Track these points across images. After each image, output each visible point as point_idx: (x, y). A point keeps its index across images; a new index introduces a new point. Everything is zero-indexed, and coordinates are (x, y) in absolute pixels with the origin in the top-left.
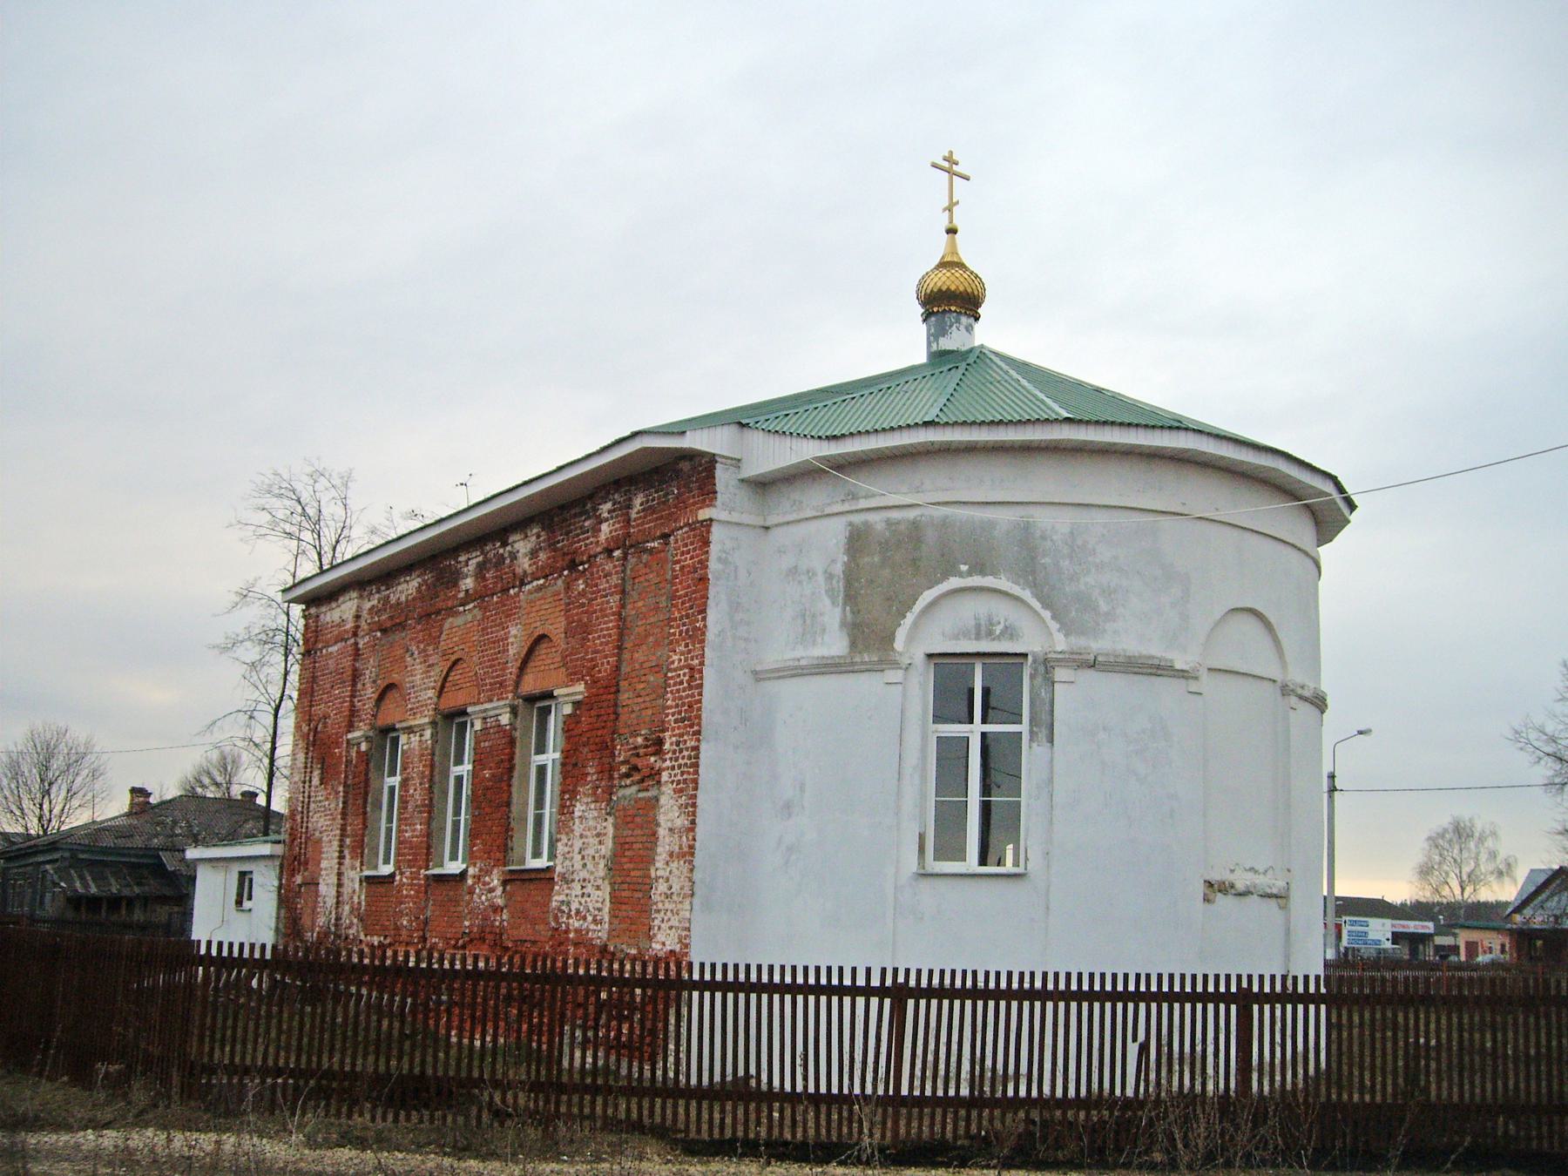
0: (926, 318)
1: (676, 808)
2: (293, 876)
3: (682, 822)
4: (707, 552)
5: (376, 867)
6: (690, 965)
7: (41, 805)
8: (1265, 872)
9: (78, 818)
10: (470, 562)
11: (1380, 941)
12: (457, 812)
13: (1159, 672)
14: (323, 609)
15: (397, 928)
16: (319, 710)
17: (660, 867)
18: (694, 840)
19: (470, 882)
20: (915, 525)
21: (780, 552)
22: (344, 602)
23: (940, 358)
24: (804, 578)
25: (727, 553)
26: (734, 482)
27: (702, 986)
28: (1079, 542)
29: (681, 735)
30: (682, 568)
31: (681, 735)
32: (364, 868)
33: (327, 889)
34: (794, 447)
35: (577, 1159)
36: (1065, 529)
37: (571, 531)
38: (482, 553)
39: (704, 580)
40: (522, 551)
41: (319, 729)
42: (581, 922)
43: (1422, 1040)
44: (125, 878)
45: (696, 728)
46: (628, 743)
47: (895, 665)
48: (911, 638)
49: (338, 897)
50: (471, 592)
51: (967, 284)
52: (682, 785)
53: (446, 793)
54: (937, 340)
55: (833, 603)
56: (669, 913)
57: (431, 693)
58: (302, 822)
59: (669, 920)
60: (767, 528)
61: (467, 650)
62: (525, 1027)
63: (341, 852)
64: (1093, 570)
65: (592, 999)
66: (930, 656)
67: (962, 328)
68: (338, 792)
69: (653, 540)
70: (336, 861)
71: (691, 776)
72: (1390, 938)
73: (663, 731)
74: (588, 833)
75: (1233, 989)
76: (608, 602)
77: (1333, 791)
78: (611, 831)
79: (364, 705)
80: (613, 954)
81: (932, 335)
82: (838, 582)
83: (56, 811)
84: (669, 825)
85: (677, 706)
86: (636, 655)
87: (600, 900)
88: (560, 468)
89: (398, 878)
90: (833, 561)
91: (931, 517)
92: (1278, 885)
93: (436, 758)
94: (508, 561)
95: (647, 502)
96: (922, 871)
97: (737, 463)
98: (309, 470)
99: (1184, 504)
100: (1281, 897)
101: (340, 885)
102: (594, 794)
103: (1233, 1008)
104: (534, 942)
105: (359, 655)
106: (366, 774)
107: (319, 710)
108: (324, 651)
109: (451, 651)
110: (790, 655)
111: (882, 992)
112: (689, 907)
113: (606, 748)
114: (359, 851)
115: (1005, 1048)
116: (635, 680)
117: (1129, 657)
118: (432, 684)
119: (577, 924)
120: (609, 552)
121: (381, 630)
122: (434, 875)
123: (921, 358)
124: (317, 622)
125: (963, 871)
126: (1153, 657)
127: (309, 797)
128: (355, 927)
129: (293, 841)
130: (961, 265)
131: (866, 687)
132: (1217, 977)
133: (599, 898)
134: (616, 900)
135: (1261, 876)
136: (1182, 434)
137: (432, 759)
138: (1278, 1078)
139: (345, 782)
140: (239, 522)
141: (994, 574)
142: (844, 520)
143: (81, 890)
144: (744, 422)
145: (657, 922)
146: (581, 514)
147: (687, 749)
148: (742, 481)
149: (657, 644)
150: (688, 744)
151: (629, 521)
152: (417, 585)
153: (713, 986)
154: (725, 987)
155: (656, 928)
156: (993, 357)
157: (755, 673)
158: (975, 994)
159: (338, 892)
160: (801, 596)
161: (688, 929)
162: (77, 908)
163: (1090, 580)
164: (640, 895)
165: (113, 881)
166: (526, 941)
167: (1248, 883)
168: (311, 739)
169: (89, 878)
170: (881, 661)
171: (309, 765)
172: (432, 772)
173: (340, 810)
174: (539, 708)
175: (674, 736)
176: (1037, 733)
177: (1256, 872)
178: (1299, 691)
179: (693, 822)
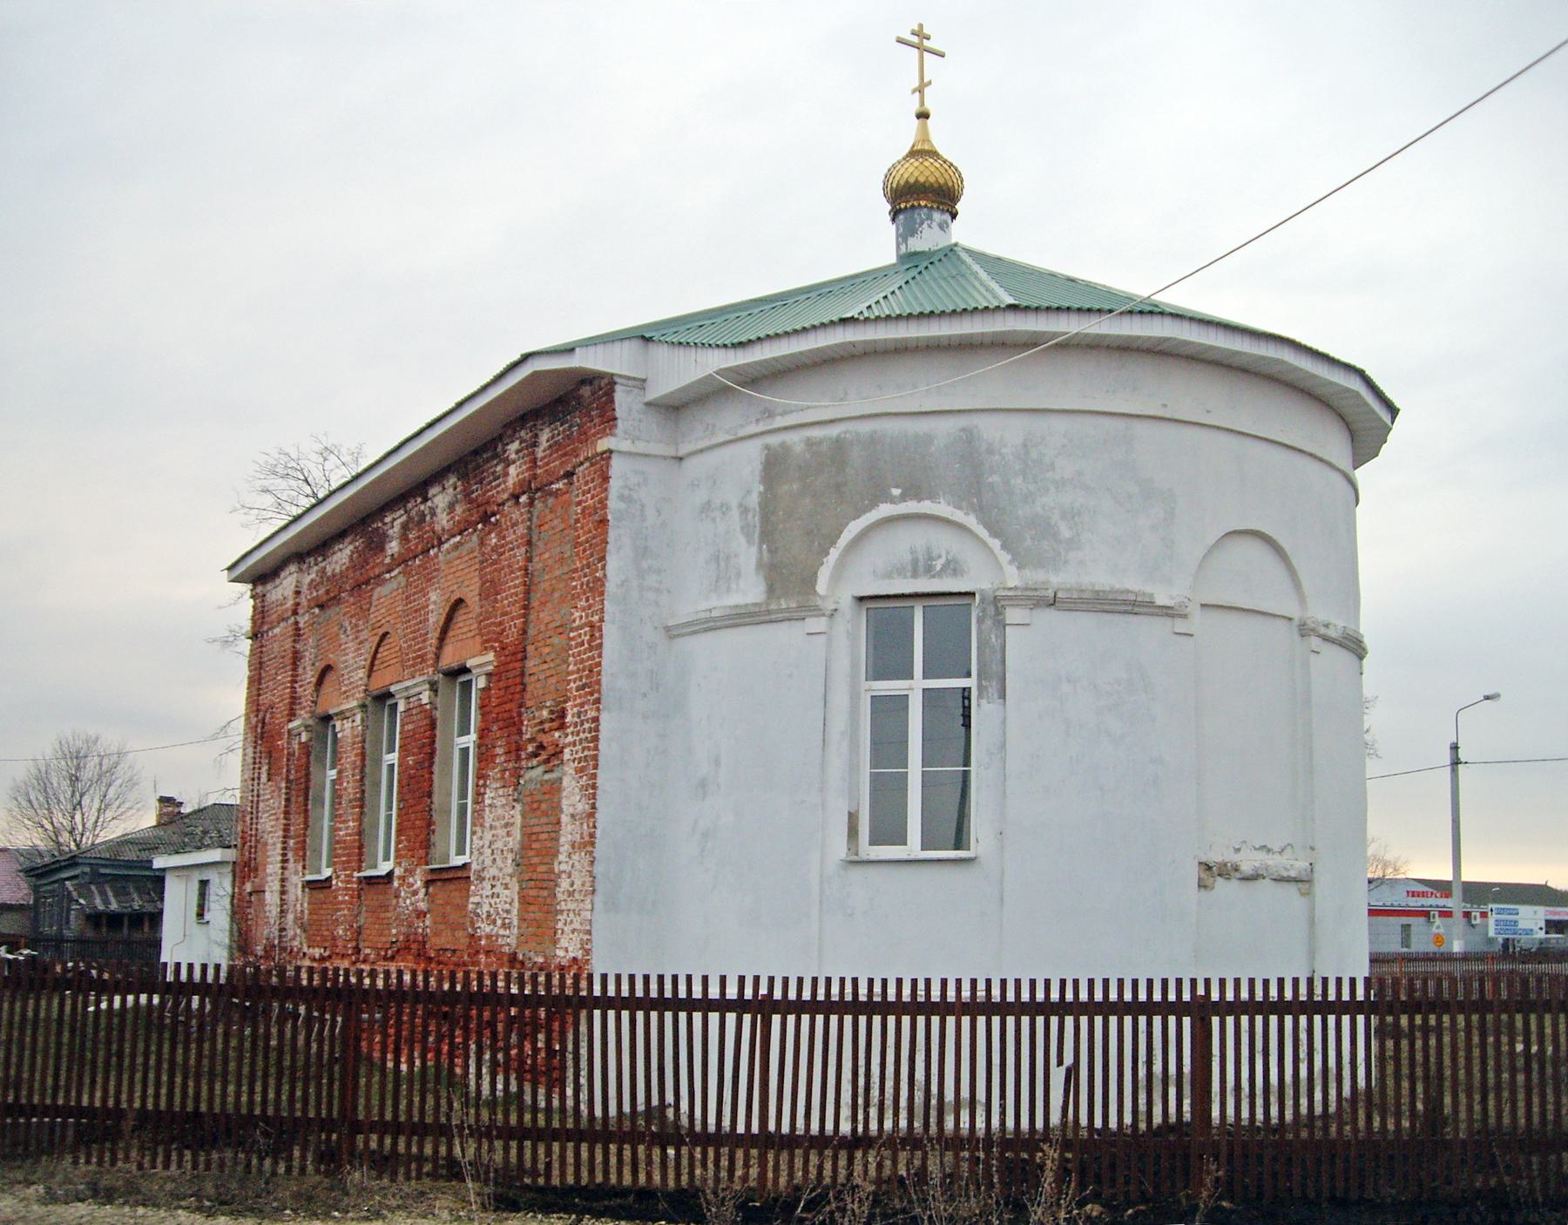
0: (895, 214)
1: (577, 790)
2: (244, 883)
3: (583, 807)
4: (606, 489)
5: (319, 872)
6: (590, 977)
7: (73, 818)
8: (1281, 852)
9: (113, 831)
10: (394, 522)
11: (1532, 930)
12: (390, 808)
13: (1136, 610)
14: (269, 586)
15: (334, 938)
16: (265, 699)
17: (563, 863)
18: (595, 827)
19: (396, 884)
20: (839, 445)
21: (693, 485)
22: (285, 578)
23: (910, 260)
24: (717, 514)
25: (630, 489)
26: (641, 406)
27: (605, 1003)
28: (1034, 455)
29: (582, 705)
30: (584, 510)
31: (582, 705)
32: (307, 872)
33: (271, 898)
34: (699, 360)
35: (350, 1215)
37: (484, 479)
38: (406, 512)
39: (603, 522)
40: (441, 505)
41: (267, 720)
42: (491, 927)
43: (1519, 1047)
44: (149, 894)
45: (596, 695)
46: (534, 718)
47: (817, 611)
48: (837, 577)
49: (282, 905)
50: (396, 556)
51: (938, 174)
52: (582, 764)
53: (378, 784)
54: (905, 241)
55: (748, 542)
56: (571, 915)
57: (361, 673)
58: (252, 824)
59: (571, 922)
60: (681, 459)
61: (392, 622)
62: (445, 1048)
63: (284, 855)
65: (501, 1016)
66: (861, 599)
67: (934, 225)
68: (280, 789)
69: (558, 480)
70: (279, 865)
71: (592, 753)
72: (1543, 926)
73: (565, 702)
74: (497, 824)
75: (1186, 997)
76: (515, 556)
77: (1457, 763)
78: (518, 820)
79: (305, 690)
80: (522, 963)
81: (901, 236)
82: (754, 517)
83: (89, 825)
84: (571, 810)
85: (578, 671)
86: (541, 615)
87: (509, 900)
88: (460, 405)
89: (334, 882)
90: (749, 492)
91: (858, 434)
92: (1298, 866)
93: (367, 746)
94: (428, 518)
95: (553, 437)
96: (855, 858)
97: (641, 383)
98: (319, 447)
99: (1165, 406)
100: (1303, 882)
101: (283, 892)
102: (503, 777)
103: (1187, 1021)
104: (454, 951)
105: (299, 635)
106: (308, 768)
107: (265, 699)
108: (270, 634)
109: (379, 624)
110: (704, 605)
111: (740, 1006)
112: (589, 907)
113: (513, 725)
114: (301, 854)
116: (540, 644)
117: (1098, 592)
118: (363, 663)
119: (488, 929)
120: (516, 497)
121: (318, 606)
122: (365, 878)
123: (890, 258)
124: (263, 601)
125: (904, 856)
126: (1128, 591)
127: (258, 796)
128: (298, 939)
129: (244, 844)
130: (934, 154)
131: (785, 638)
132: (1165, 982)
133: (508, 897)
134: (525, 901)
135: (1277, 856)
136: (1157, 321)
137: (363, 748)
139: (288, 776)
140: (243, 506)
141: (932, 497)
142: (758, 443)
143: (101, 907)
144: (647, 335)
145: (560, 925)
146: (493, 458)
147: (587, 721)
148: (649, 404)
149: (562, 600)
150: (589, 716)
151: (534, 461)
152: (349, 553)
153: (618, 1003)
154: (647, 1004)
155: (560, 932)
156: (968, 260)
157: (667, 629)
158: (856, 1008)
159: (282, 900)
160: (715, 535)
161: (589, 932)
162: (97, 926)
164: (545, 893)
165: (135, 896)
166: (446, 950)
167: (1257, 864)
168: (259, 730)
169: (110, 894)
170: (800, 607)
171: (257, 760)
172: (363, 760)
173: (282, 809)
174: (461, 683)
175: (576, 706)
176: (986, 687)
177: (1269, 850)
178: (1323, 631)
179: (594, 807)
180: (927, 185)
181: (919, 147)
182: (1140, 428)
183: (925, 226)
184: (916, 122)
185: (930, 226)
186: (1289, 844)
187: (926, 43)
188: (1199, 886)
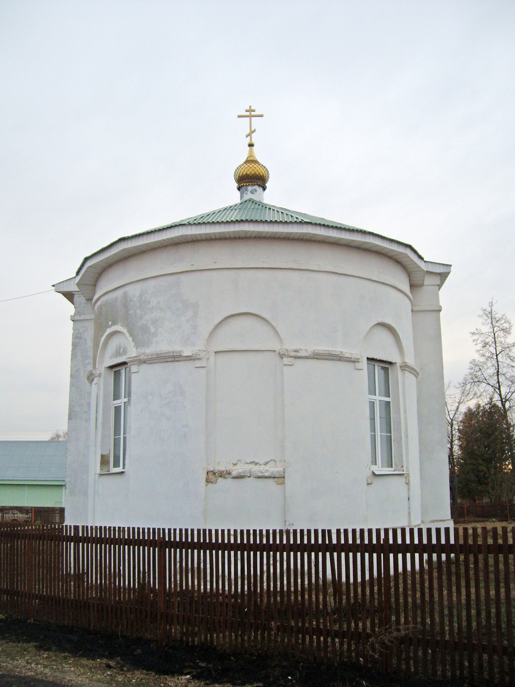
13: (176, 359)
28: (143, 299)
36: (138, 294)
64: (149, 312)
99: (192, 265)
117: (158, 354)
130: (256, 162)
138: (265, 584)
163: (147, 317)
180: (251, 175)
182: (183, 277)
183: (245, 194)
184: (249, 148)
186: (274, 460)
187: (253, 113)
188: (206, 481)
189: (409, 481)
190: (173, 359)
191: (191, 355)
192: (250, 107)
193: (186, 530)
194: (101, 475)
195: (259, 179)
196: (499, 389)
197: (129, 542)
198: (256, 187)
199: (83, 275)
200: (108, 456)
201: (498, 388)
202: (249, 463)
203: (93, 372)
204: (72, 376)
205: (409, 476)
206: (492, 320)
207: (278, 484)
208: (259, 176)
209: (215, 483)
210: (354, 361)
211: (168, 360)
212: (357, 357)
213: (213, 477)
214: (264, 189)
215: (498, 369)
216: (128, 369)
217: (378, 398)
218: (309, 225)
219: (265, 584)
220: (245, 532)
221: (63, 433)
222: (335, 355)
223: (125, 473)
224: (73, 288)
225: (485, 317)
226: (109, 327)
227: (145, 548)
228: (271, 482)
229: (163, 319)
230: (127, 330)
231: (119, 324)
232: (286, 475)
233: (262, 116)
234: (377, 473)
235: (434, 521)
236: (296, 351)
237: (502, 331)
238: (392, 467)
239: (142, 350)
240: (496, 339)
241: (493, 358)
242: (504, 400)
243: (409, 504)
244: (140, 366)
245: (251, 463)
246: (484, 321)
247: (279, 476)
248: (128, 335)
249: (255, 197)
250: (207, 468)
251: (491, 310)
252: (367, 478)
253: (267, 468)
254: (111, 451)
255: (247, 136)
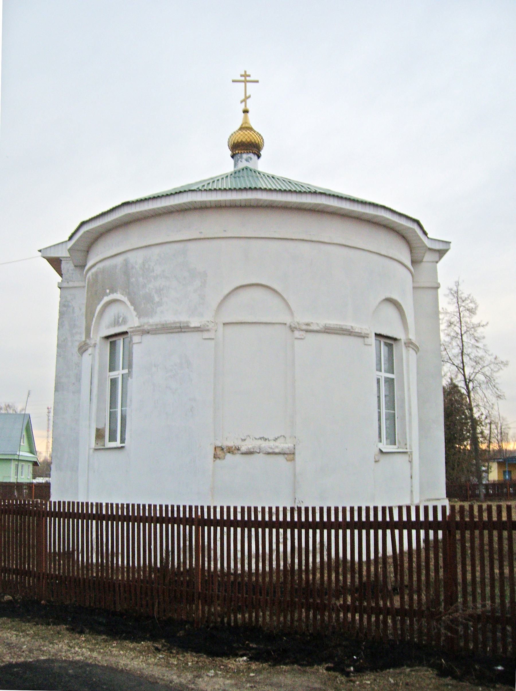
13: (183, 330)
28: (147, 266)
36: (140, 261)
75: (440, 518)
115: (403, 538)
117: (163, 325)
130: (251, 129)
138: (274, 563)
163: (151, 286)
181: (244, 126)
182: (191, 245)
183: (239, 161)
185: (241, 161)
186: (284, 436)
187: (248, 79)
188: (214, 457)
189: (412, 459)
190: (180, 330)
191: (199, 325)
192: (245, 72)
193: (173, 507)
194: (96, 450)
195: (255, 147)
196: (463, 370)
197: (161, 520)
198: (251, 155)
199: (78, 241)
200: (104, 430)
201: (462, 368)
202: (259, 439)
203: (88, 341)
204: (58, 346)
205: (412, 454)
206: (458, 299)
207: (287, 460)
208: (255, 144)
209: (223, 459)
210: (363, 336)
211: (174, 330)
212: (367, 332)
213: (220, 453)
214: (259, 157)
215: (463, 349)
216: (127, 340)
217: (384, 375)
218: (322, 195)
219: (274, 563)
220: (253, 509)
221: (5, 405)
222: (346, 330)
223: (125, 448)
224: (62, 253)
225: (451, 297)
226: (107, 295)
227: (135, 524)
228: (281, 458)
229: (169, 288)
230: (128, 298)
231: (119, 292)
232: (297, 452)
233: (257, 82)
234: (384, 450)
235: (429, 500)
236: (308, 325)
237: (468, 312)
238: (395, 444)
239: (144, 320)
240: (461, 319)
241: (458, 338)
242: (468, 381)
243: (411, 482)
244: (143, 336)
245: (261, 438)
246: (450, 301)
247: (289, 452)
248: (128, 304)
249: (250, 165)
250: (215, 443)
251: (457, 290)
252: (375, 455)
253: (277, 444)
254: (106, 425)
255: (242, 102)
